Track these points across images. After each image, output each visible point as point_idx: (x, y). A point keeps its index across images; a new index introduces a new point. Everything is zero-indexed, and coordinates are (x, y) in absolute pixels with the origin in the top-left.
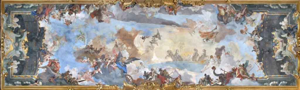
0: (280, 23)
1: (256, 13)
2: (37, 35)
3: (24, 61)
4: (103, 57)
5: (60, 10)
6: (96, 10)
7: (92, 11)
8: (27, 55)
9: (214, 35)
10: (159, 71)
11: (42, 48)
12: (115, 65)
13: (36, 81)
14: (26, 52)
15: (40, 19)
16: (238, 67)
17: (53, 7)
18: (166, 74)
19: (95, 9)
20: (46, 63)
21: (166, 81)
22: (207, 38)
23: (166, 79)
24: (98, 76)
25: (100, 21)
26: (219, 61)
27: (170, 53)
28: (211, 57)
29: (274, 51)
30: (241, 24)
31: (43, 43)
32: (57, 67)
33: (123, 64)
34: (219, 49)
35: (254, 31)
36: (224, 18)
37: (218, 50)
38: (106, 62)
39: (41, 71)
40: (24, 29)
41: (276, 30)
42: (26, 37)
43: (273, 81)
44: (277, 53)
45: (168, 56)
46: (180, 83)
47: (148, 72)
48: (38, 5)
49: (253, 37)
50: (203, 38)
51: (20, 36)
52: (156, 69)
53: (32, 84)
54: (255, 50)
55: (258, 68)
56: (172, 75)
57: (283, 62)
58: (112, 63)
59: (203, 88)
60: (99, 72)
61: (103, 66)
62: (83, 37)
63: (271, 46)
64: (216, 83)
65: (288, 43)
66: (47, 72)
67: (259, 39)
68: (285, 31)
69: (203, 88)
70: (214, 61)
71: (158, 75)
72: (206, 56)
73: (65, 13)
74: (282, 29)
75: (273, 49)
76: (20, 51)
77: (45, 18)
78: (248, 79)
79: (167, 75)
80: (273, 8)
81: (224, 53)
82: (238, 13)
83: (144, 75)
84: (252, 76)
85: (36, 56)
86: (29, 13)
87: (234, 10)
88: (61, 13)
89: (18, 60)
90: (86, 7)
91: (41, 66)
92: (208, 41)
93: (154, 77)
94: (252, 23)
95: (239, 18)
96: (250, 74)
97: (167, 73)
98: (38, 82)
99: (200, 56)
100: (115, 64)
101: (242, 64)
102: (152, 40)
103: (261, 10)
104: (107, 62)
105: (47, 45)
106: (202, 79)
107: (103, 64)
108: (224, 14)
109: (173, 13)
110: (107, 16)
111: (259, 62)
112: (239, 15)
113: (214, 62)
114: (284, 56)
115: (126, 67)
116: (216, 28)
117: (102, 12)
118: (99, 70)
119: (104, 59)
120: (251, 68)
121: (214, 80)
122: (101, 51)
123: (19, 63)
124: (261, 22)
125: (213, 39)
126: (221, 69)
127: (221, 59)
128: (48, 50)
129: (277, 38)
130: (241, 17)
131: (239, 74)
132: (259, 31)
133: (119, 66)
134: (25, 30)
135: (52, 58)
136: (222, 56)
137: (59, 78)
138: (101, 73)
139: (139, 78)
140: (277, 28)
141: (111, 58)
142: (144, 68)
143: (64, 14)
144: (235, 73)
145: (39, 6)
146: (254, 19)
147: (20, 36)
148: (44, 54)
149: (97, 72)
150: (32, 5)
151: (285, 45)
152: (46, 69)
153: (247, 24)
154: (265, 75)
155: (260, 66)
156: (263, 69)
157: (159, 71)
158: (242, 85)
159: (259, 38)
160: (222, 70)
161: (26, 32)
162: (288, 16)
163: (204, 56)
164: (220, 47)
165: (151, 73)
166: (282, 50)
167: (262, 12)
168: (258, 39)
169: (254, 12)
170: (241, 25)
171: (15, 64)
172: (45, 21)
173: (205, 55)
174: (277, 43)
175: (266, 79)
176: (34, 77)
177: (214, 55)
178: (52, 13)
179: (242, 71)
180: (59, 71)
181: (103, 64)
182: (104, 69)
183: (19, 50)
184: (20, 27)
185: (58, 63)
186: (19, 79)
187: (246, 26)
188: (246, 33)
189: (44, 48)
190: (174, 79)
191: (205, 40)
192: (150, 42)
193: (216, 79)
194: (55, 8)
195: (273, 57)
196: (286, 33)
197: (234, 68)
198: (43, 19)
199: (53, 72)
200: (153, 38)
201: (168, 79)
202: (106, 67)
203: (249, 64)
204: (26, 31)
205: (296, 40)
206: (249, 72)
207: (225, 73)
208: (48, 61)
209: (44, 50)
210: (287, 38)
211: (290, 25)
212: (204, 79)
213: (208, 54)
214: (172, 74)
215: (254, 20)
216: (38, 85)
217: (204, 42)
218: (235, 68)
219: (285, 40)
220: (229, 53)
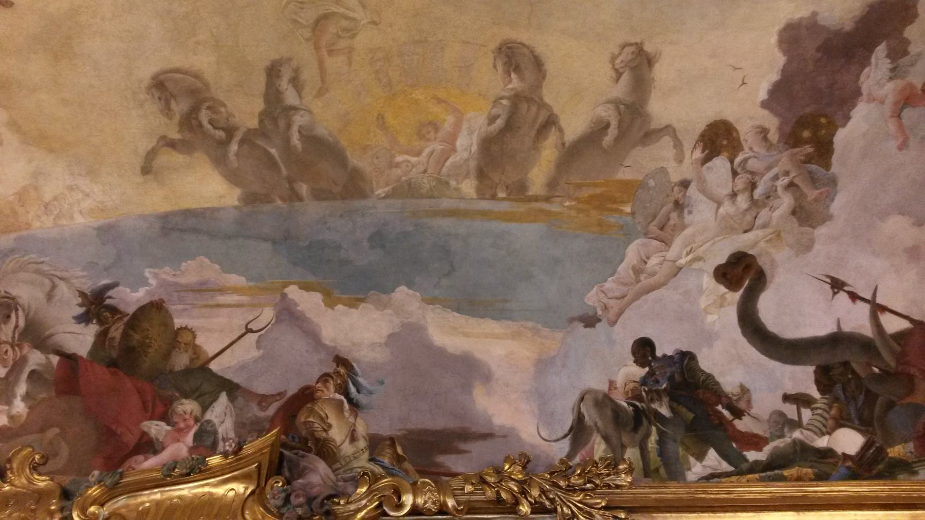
18: (167, 356)
21: (156, 429)
23: (168, 403)
26: (812, 194)
46: (347, 449)
52: (50, 297)
56: (243, 367)
64: (797, 434)
70: (753, 186)
71: (69, 359)
72: (649, 136)
79: (181, 361)
81: (890, 90)
97: (178, 338)
99: (574, 125)
106: (603, 401)
126: (837, 285)
127: (835, 168)
136: (858, 129)
160: (843, 297)
173: (632, 121)
190: (263, 400)
193: (787, 398)
201: (188, 406)
213: (680, 105)
214: (247, 351)
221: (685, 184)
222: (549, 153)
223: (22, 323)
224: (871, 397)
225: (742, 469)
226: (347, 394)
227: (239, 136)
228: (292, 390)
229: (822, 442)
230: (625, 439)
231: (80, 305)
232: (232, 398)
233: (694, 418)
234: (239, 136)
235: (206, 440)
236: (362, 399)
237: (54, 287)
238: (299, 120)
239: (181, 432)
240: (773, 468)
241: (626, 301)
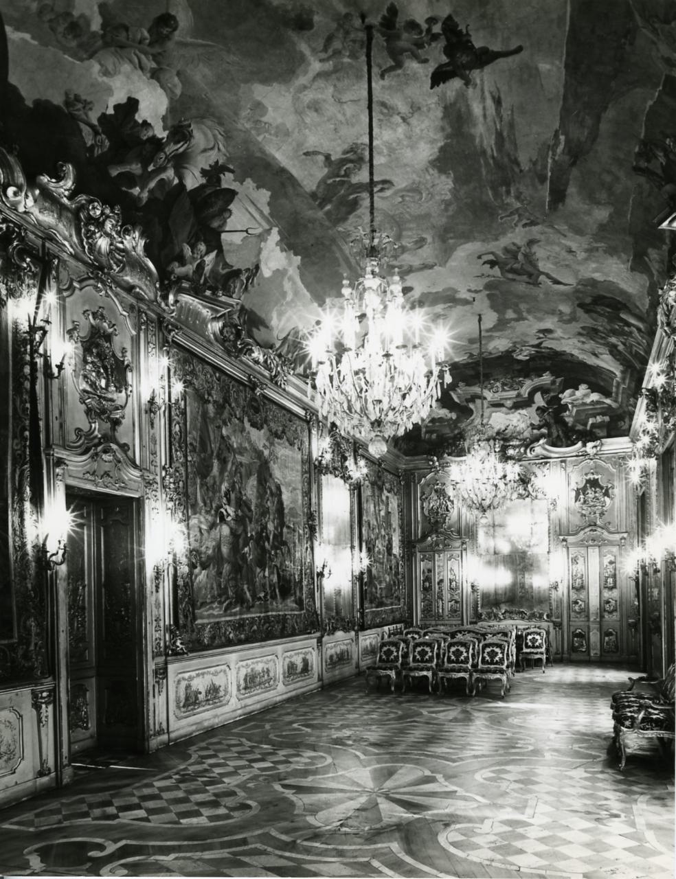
10: (204, 172)
18: (213, 217)
21: (187, 251)
23: (198, 240)
27: (351, 161)
45: (328, 157)
47: (146, 124)
52: (205, 151)
59: (453, 670)
69: (453, 670)
71: (181, 185)
79: (215, 224)
83: (103, 118)
97: (225, 212)
102: (413, 25)
114: (471, 406)
139: (58, 100)
151: (509, 403)
157: (204, 172)
165: (157, 144)
166: (489, 399)
190: (226, 265)
192: (393, 11)
200: (437, 29)
201: (202, 247)
211: (575, 410)
214: (237, 238)
223: (181, 150)
226: (247, 281)
227: (346, 179)
231: (210, 166)
232: (217, 256)
234: (346, 179)
236: (250, 287)
237: (212, 149)
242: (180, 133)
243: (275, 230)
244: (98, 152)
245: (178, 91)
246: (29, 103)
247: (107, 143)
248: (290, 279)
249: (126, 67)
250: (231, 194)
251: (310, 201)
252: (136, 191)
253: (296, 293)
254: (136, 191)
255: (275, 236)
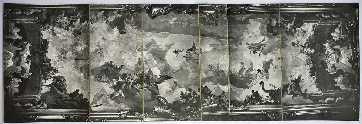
0: (332, 34)
1: (307, 23)
2: (40, 48)
3: (26, 78)
4: (124, 76)
5: (69, 18)
6: (118, 18)
7: (111, 19)
8: (30, 71)
9: (262, 47)
11: (45, 64)
12: (139, 87)
13: (39, 103)
14: (29, 68)
15: (43, 29)
16: (290, 83)
17: (61, 13)
18: (207, 92)
19: (117, 17)
20: (50, 81)
21: (206, 100)
22: (254, 50)
23: (207, 97)
24: (119, 99)
25: (122, 33)
26: (267, 76)
27: (212, 68)
28: (259, 71)
29: (326, 64)
30: (292, 36)
31: (46, 58)
32: (63, 85)
33: (154, 84)
34: (267, 62)
35: (306, 44)
36: (274, 29)
37: (265, 63)
38: (128, 82)
39: (45, 90)
40: (26, 40)
41: (328, 41)
42: (28, 50)
43: (328, 97)
44: (329, 66)
46: (225, 102)
48: (40, 11)
49: (305, 49)
50: (251, 50)
51: (21, 49)
52: (195, 89)
53: (34, 107)
54: (308, 63)
55: (311, 83)
56: (214, 93)
57: (337, 75)
58: (135, 84)
60: (120, 95)
61: (125, 87)
62: (101, 51)
63: (324, 59)
64: (267, 100)
65: (341, 55)
66: (52, 91)
67: (311, 52)
68: (338, 42)
70: (262, 75)
72: (253, 70)
73: (75, 21)
74: (334, 40)
75: (325, 62)
76: (22, 67)
77: (48, 27)
78: (300, 96)
80: (325, 18)
81: (272, 67)
82: (287, 24)
84: (304, 92)
85: (39, 72)
86: (31, 21)
87: (282, 20)
88: (70, 22)
89: (19, 78)
90: (104, 14)
91: (45, 84)
92: (256, 53)
93: (195, 99)
94: (304, 35)
95: (290, 29)
96: (303, 90)
98: (41, 104)
99: (247, 69)
100: (138, 85)
101: (294, 80)
102: (187, 55)
103: (312, 20)
104: (130, 83)
105: (50, 60)
106: (248, 97)
107: (125, 85)
108: (275, 25)
109: (213, 23)
110: (131, 27)
111: (312, 76)
112: (289, 26)
113: (262, 76)
114: (338, 69)
115: (158, 87)
116: (264, 40)
117: (126, 22)
118: (121, 91)
119: (126, 79)
120: (304, 83)
121: (264, 97)
122: (122, 68)
123: (20, 81)
124: (313, 33)
125: (260, 52)
126: (271, 85)
127: (269, 74)
128: (52, 65)
129: (329, 50)
130: (291, 28)
131: (291, 91)
132: (311, 43)
133: (149, 86)
134: (27, 42)
135: (57, 75)
136: (271, 71)
137: (68, 99)
138: (122, 96)
139: (175, 100)
140: (329, 40)
141: (134, 77)
142: (180, 87)
143: (74, 23)
144: (287, 90)
145: (42, 12)
146: (305, 30)
147: (21, 49)
148: (48, 70)
149: (118, 95)
150: (33, 11)
151: (337, 56)
152: (50, 88)
153: (298, 35)
154: (319, 91)
155: (313, 81)
156: (317, 83)
158: (293, 103)
159: (312, 50)
160: (271, 86)
161: (28, 44)
162: (339, 26)
163: (251, 70)
164: (267, 60)
165: (189, 94)
166: (335, 63)
167: (313, 22)
168: (310, 52)
169: (305, 22)
170: (293, 37)
171: (14, 83)
172: (49, 31)
173: (252, 69)
174: (330, 55)
175: (320, 96)
176: (37, 98)
177: (261, 69)
178: (59, 21)
179: (295, 87)
180: (66, 90)
181: (125, 85)
182: (126, 91)
183: (21, 66)
184: (21, 38)
185: (64, 80)
186: (24, 100)
187: (298, 37)
188: (298, 46)
189: (47, 63)
190: (216, 96)
191: (252, 52)
193: (266, 96)
194: (63, 14)
195: (326, 70)
196: (338, 44)
197: (286, 84)
198: (46, 28)
199: (59, 92)
200: (188, 52)
201: (209, 97)
202: (128, 88)
203: (302, 79)
204: (28, 43)
205: (351, 50)
206: (301, 87)
207: (275, 89)
208: (53, 79)
209: (47, 66)
210: (339, 50)
212: (252, 96)
213: (256, 68)
214: (215, 91)
215: (305, 32)
216: (42, 107)
217: (252, 54)
218: (287, 84)
219: (338, 52)
220: (278, 67)
221: (257, 75)
222: (245, 71)
224: (275, 96)
225: (262, 104)
228: (219, 95)
229: (269, 101)
230: (250, 101)
233: (188, 103)
235: (211, 101)
238: (220, 68)
239: (209, 100)
240: (265, 104)
241: (252, 86)
242: (190, 90)
243: (219, 85)
244: (184, 101)
245: (184, 86)
246: (172, 103)
247: (184, 99)
248: (234, 89)
249: (177, 90)
250: (206, 87)
251: (216, 77)
252: (194, 102)
253: (239, 91)
254: (194, 102)
255: (220, 86)
